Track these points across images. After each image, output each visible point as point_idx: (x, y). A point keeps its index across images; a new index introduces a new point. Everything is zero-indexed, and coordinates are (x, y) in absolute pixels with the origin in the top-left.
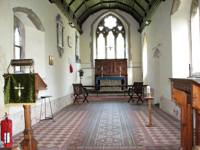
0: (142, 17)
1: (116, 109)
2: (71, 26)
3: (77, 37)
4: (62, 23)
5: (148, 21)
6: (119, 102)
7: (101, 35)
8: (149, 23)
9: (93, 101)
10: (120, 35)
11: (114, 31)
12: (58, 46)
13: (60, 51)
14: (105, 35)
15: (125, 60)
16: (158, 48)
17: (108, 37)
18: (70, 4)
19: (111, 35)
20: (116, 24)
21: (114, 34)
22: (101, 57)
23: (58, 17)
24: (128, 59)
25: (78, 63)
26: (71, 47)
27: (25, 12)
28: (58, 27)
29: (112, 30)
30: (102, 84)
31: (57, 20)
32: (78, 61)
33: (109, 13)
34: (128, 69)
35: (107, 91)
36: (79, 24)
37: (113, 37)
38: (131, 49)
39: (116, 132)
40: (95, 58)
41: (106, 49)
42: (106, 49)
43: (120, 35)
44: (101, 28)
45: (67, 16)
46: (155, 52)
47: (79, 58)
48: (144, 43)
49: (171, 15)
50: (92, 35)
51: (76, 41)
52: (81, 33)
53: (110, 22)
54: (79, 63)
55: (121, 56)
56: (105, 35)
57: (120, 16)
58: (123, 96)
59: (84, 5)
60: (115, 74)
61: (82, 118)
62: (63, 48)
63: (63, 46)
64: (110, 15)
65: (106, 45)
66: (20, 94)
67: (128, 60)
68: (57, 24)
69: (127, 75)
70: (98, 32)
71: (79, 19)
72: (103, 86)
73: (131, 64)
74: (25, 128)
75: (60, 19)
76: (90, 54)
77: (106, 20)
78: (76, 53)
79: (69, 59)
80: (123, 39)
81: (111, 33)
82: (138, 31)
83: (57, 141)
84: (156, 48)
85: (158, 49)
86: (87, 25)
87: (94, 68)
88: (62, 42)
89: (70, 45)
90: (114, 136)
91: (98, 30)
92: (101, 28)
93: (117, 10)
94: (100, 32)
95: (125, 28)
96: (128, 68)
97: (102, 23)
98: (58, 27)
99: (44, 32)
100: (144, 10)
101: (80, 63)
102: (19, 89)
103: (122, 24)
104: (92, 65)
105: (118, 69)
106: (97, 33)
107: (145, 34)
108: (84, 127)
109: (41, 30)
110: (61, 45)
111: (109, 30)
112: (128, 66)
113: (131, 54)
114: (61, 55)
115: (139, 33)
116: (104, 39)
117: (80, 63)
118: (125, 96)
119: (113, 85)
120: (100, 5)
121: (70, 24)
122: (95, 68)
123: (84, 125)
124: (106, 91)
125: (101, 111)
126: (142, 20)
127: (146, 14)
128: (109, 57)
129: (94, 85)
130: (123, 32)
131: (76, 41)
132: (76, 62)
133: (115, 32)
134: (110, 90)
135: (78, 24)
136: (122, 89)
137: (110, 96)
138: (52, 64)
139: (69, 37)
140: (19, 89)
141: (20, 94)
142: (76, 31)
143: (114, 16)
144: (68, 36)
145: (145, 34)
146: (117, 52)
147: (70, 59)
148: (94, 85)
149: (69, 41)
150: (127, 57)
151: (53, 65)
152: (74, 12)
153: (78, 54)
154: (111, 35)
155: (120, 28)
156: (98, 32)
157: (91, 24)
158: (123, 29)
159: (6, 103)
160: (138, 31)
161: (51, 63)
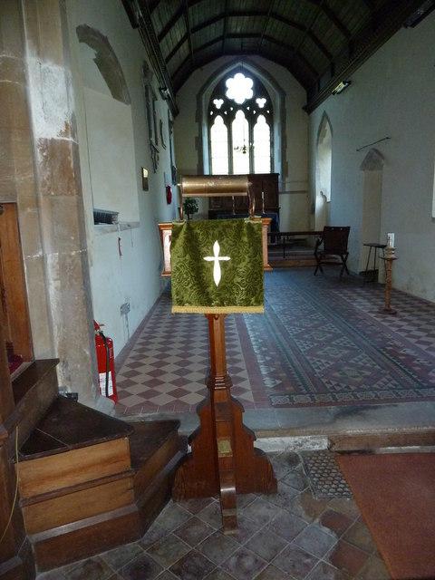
0: (317, 74)
7: (219, 120)
10: (261, 119)
11: (248, 108)
12: (151, 144)
14: (228, 120)
15: (272, 177)
17: (234, 124)
19: (240, 119)
29: (243, 107)
33: (239, 64)
34: (280, 196)
37: (246, 123)
41: (251, 149)
43: (261, 119)
50: (199, 120)
53: (240, 87)
55: (263, 167)
56: (228, 120)
57: (264, 72)
59: (185, 45)
61: (150, 321)
67: (279, 177)
73: (287, 185)
77: (229, 83)
80: (267, 127)
81: (240, 115)
91: (212, 107)
92: (218, 103)
93: (257, 59)
94: (218, 112)
96: (282, 193)
97: (220, 91)
100: (329, 56)
107: (325, 116)
109: (123, 101)
110: (153, 139)
111: (237, 107)
112: (280, 190)
120: (219, 44)
127: (333, 65)
143: (247, 74)
145: (325, 116)
146: (256, 159)
150: (278, 170)
154: (240, 119)
155: (261, 102)
156: (212, 113)
158: (268, 105)
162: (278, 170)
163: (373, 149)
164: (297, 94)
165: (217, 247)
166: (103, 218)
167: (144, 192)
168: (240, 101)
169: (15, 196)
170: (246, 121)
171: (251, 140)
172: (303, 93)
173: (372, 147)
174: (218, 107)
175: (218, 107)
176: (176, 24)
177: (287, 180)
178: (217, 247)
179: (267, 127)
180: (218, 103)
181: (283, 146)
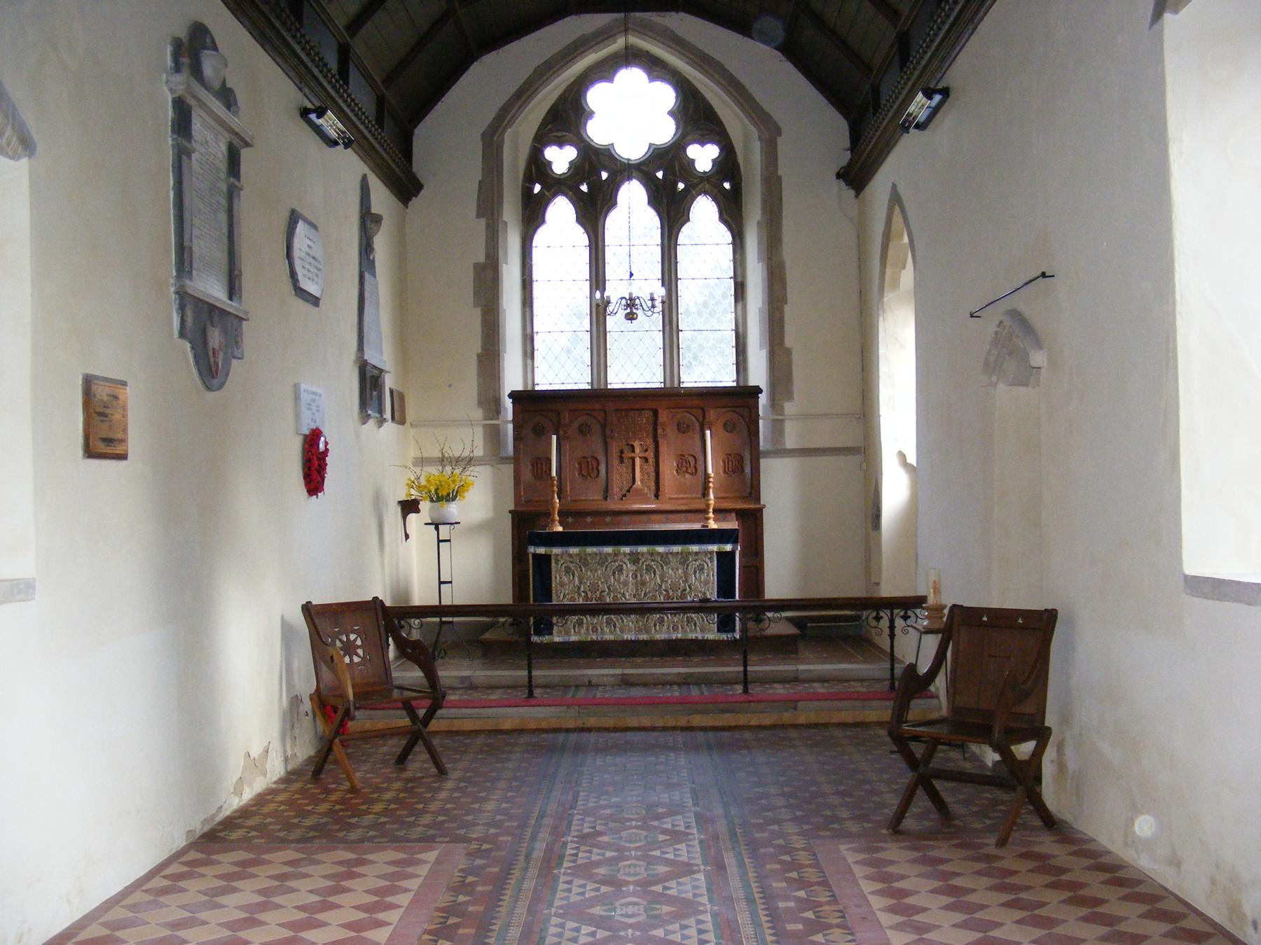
1: (683, 852)
2: (318, 130)
3: (369, 221)
4: (227, 96)
5: (929, 94)
6: (700, 736)
7: (561, 211)
8: (935, 111)
9: (498, 740)
10: (704, 210)
13: (210, 338)
14: (594, 211)
15: (739, 399)
16: (1022, 308)
17: (614, 223)
18: (355, 25)
19: (633, 207)
21: (654, 201)
22: (561, 367)
24: (763, 386)
25: (381, 422)
26: (315, 301)
27: (487, 256)
29: (641, 170)
30: (565, 588)
32: (381, 411)
33: (620, 43)
34: (764, 463)
36: (388, 123)
37: (649, 222)
38: (787, 308)
39: (665, 832)
40: (512, 380)
41: (599, 311)
43: (704, 210)
44: (560, 158)
45: (318, 89)
46: (996, 340)
47: (389, 382)
48: (889, 271)
49: (1158, 15)
50: (489, 207)
51: (366, 249)
52: (406, 187)
53: (631, 111)
54: (389, 426)
55: (710, 367)
56: (594, 211)
57: (705, 62)
58: (727, 682)
60: (667, 507)
63: (233, 290)
64: (630, 57)
65: (598, 278)
67: (763, 399)
69: (760, 511)
70: (537, 188)
71: (389, 79)
73: (790, 424)
74: (779, 139)
76: (478, 349)
77: (596, 96)
81: (633, 194)
82: (839, 176)
83: (278, 906)
84: (1006, 305)
86: (449, 134)
87: (504, 460)
88: (221, 256)
90: (656, 883)
91: (538, 168)
92: (560, 158)
94: (556, 185)
95: (741, 161)
96: (768, 454)
97: (567, 118)
99: (25, 161)
101: (399, 417)
103: (720, 124)
104: (494, 435)
105: (690, 464)
106: (527, 192)
107: (896, 199)
108: (451, 800)
111: (623, 171)
114: (211, 370)
115: (852, 193)
116: (580, 237)
117: (402, 422)
118: (746, 681)
121: (304, 113)
122: (516, 460)
123: (453, 790)
126: (876, 92)
128: (621, 377)
129: (507, 598)
130: (727, 185)
131: (366, 249)
132: (365, 418)
133: (669, 183)
134: (628, 630)
135: (380, 121)
136: (725, 624)
137: (626, 682)
138: (119, 450)
142: (364, 179)
143: (656, 68)
144: (293, 212)
145: (896, 199)
147: (305, 398)
150: (758, 375)
151: (123, 457)
152: (341, 22)
153: (383, 356)
154: (633, 207)
155: (703, 156)
156: (537, 188)
157: (484, 126)
158: (727, 166)
160: (839, 176)
161: (102, 441)
162: (758, 375)
163: (231, 299)
164: (811, 127)
168: (632, 149)
171: (669, 275)
172: (835, 126)
173: (1006, 305)
174: (570, 153)
175: (570, 153)
177: (789, 408)
179: (724, 235)
181: (774, 294)
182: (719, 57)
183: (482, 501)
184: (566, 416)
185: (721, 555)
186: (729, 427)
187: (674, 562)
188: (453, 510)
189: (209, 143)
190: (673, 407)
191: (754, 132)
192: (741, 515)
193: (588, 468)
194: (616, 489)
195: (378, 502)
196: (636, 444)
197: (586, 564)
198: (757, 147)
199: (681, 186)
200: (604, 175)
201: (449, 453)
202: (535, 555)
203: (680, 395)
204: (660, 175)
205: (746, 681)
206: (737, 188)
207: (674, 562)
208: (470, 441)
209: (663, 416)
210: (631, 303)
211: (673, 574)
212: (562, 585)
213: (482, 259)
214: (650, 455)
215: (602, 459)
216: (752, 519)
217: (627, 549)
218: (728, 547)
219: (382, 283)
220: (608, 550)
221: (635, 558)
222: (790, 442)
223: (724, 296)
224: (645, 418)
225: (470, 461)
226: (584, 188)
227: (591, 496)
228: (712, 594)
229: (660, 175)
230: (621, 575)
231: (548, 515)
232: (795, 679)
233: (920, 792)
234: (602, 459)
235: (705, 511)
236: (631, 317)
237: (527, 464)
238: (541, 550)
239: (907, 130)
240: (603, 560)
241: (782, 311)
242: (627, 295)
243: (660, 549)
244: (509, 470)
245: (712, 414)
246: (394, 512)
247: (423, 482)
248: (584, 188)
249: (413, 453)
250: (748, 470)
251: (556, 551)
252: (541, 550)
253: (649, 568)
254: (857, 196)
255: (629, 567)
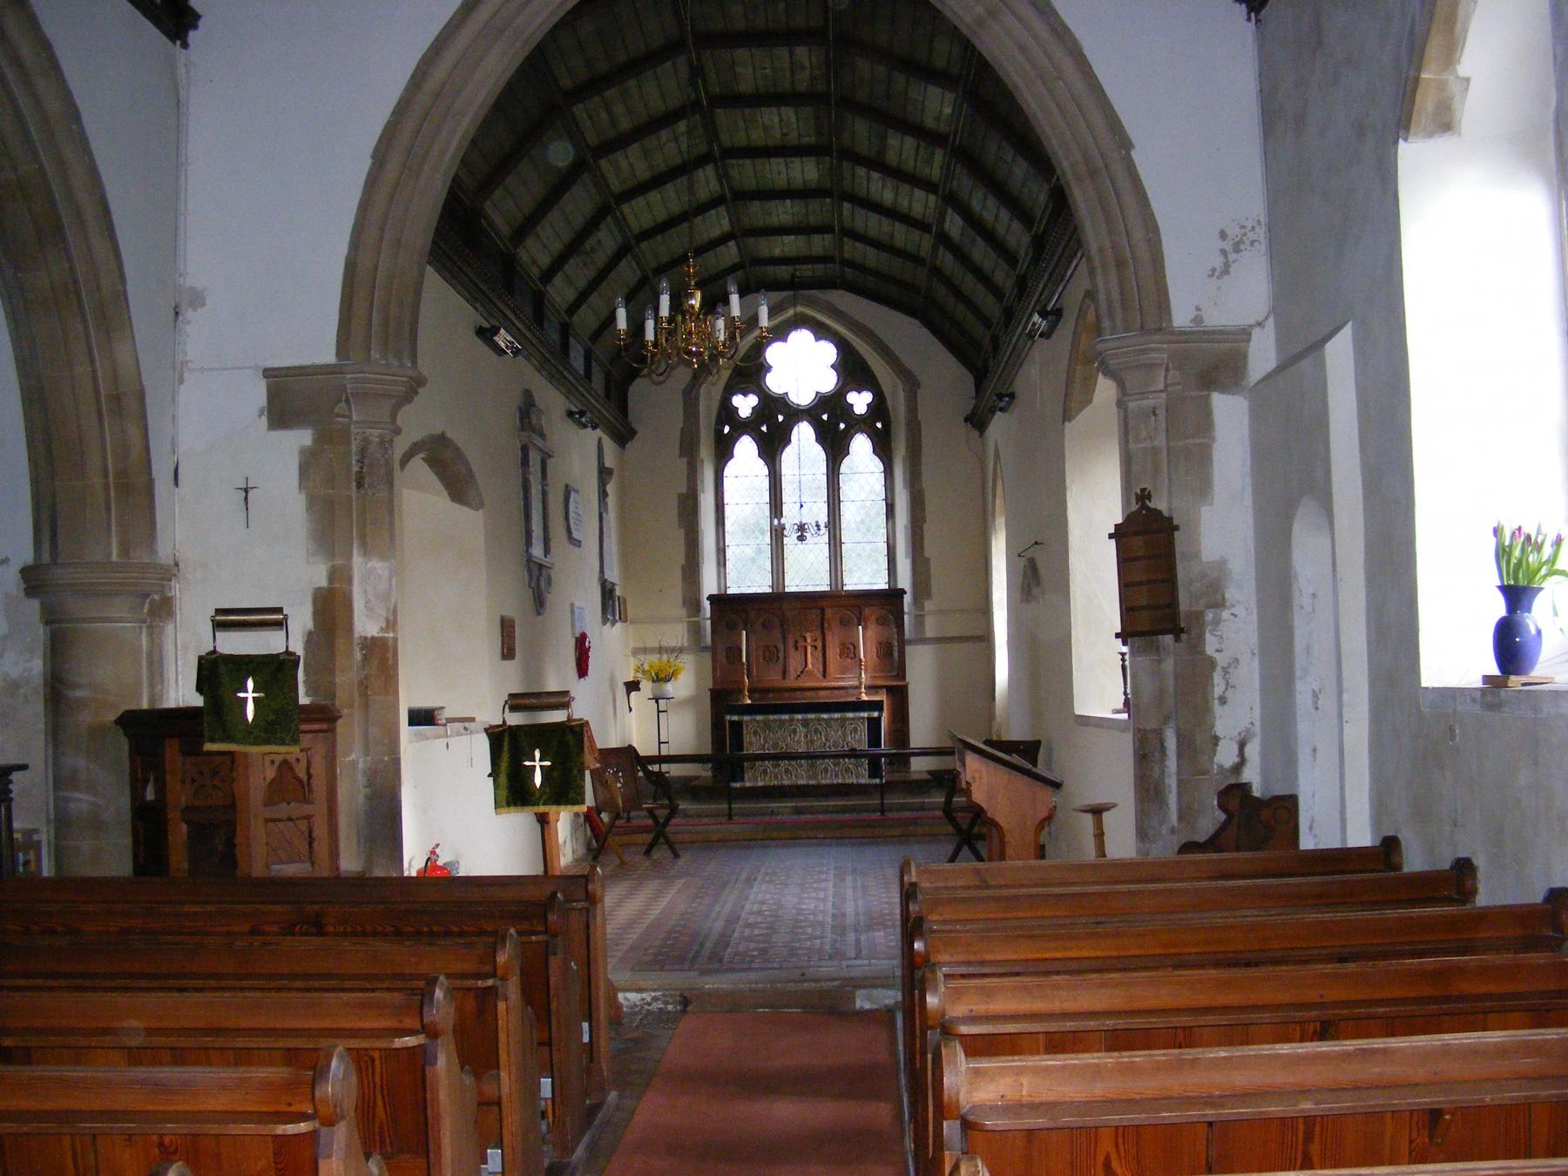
3: (604, 473)
7: (746, 448)
10: (861, 445)
12: (529, 558)
14: (771, 448)
15: (891, 597)
17: (788, 457)
20: (834, 373)
22: (747, 574)
23: (527, 411)
25: (614, 623)
28: (525, 462)
30: (753, 743)
31: (522, 428)
33: (791, 312)
34: (908, 649)
35: (786, 782)
37: (817, 455)
38: (926, 527)
40: (709, 587)
41: (778, 534)
42: (778, 534)
43: (861, 445)
44: (745, 405)
47: (618, 592)
50: (689, 449)
51: (603, 495)
52: (623, 435)
53: (802, 366)
55: (866, 572)
56: (771, 448)
58: (867, 809)
62: (547, 561)
63: (547, 551)
66: (538, 780)
67: (907, 599)
68: (525, 450)
72: (763, 757)
73: (926, 620)
75: (534, 421)
78: (602, 571)
79: (573, 612)
81: (804, 433)
85: (1039, 565)
87: (704, 649)
89: (576, 535)
94: (741, 427)
96: (911, 642)
97: (751, 373)
98: (525, 462)
102: (538, 765)
104: (695, 630)
105: (849, 650)
110: (537, 551)
111: (796, 414)
113: (928, 560)
115: (977, 434)
116: (761, 469)
118: (882, 809)
119: (816, 747)
122: (713, 649)
124: (782, 787)
125: (749, 882)
128: (795, 582)
129: (707, 749)
130: (879, 425)
131: (603, 495)
132: (605, 621)
133: (833, 423)
134: (800, 776)
135: (608, 397)
136: (875, 771)
137: (799, 811)
139: (568, 491)
140: (538, 765)
141: (538, 780)
143: (821, 332)
148: (707, 749)
149: (572, 515)
150: (904, 581)
153: (613, 575)
155: (860, 401)
156: (727, 430)
158: (878, 408)
159: (497, 805)
160: (966, 420)
162: (904, 581)
165: (250, 684)
166: (422, 718)
167: (508, 663)
168: (802, 397)
169: (333, 696)
170: (819, 448)
174: (753, 400)
175: (753, 400)
176: (603, 226)
177: (929, 606)
178: (250, 684)
179: (876, 465)
180: (745, 405)
182: (871, 326)
183: (686, 683)
184: (752, 615)
185: (869, 719)
186: (881, 621)
187: (835, 725)
188: (669, 688)
189: (535, 459)
190: (836, 608)
191: (900, 387)
192: (891, 690)
193: (771, 654)
194: (792, 673)
195: (612, 680)
196: (808, 636)
197: (769, 728)
198: (901, 396)
199: (842, 426)
200: (781, 418)
201: (664, 644)
202: (732, 723)
203: (840, 596)
204: (825, 417)
205: (882, 809)
206: (887, 425)
207: (835, 725)
208: (677, 634)
209: (829, 613)
210: (802, 528)
211: (835, 734)
212: (751, 744)
213: (684, 490)
214: (819, 644)
215: (781, 646)
216: (899, 695)
217: (800, 717)
218: (876, 714)
219: (611, 517)
220: (786, 717)
221: (806, 723)
222: (929, 633)
223: (878, 514)
224: (814, 615)
225: (681, 650)
226: (764, 429)
227: (773, 678)
228: (864, 746)
229: (825, 417)
230: (797, 734)
231: (741, 691)
232: (922, 808)
233: (965, 848)
234: (781, 646)
235: (859, 687)
236: (801, 538)
237: (723, 656)
238: (735, 718)
239: (993, 413)
240: (782, 723)
241: (921, 528)
242: (801, 516)
243: (825, 716)
244: (708, 657)
245: (867, 611)
246: (622, 690)
247: (646, 667)
248: (764, 429)
249: (632, 644)
250: (896, 654)
251: (746, 718)
252: (735, 718)
253: (816, 731)
254: (981, 436)
255: (801, 730)
